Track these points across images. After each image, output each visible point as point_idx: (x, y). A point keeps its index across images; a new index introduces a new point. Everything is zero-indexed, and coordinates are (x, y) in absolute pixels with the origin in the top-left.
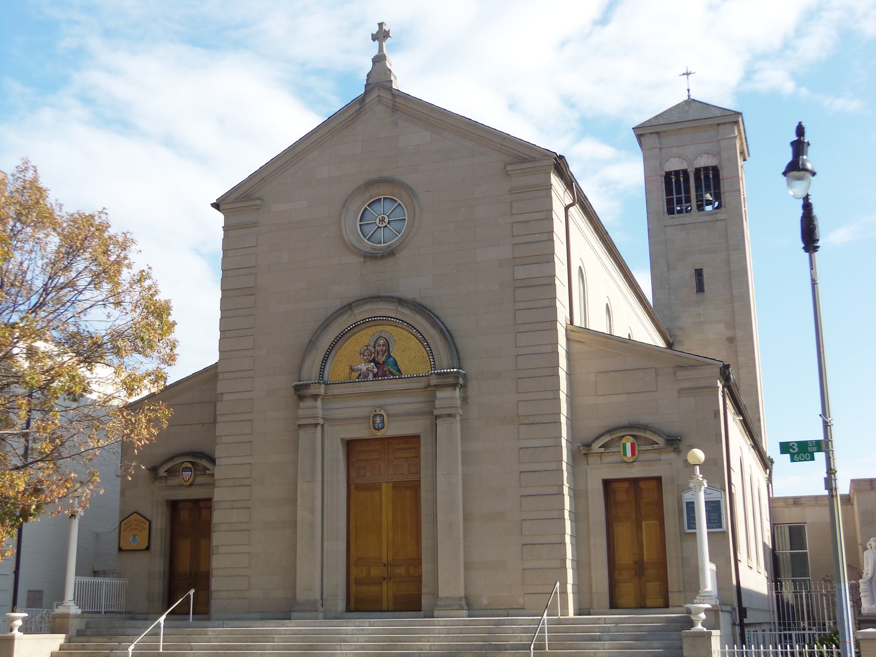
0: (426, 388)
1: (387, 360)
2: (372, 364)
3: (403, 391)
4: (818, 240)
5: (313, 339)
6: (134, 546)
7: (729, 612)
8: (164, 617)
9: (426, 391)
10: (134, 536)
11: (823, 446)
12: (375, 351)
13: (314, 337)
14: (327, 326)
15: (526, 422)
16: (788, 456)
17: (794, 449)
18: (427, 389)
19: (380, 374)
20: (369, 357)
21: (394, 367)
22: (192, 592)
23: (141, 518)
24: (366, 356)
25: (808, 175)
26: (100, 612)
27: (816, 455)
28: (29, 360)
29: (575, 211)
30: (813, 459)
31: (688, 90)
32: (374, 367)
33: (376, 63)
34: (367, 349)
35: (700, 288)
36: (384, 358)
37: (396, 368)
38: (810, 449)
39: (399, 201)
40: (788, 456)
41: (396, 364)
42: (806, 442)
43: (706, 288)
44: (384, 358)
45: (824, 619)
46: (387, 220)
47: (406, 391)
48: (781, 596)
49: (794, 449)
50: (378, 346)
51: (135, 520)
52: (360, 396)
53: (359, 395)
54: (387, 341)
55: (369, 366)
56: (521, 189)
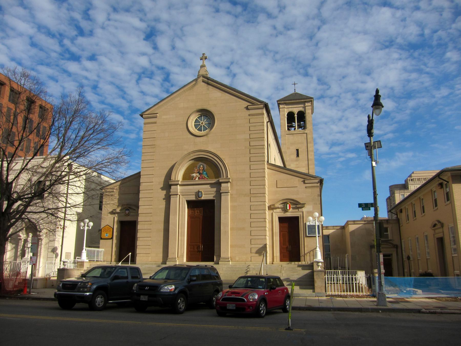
4: (373, 133)
6: (107, 237)
8: (121, 263)
10: (107, 233)
11: (374, 205)
16: (361, 208)
17: (363, 206)
19: (201, 177)
22: (130, 254)
25: (381, 107)
26: (94, 261)
27: (371, 208)
29: (269, 124)
30: (370, 209)
31: (295, 90)
33: (202, 68)
35: (298, 155)
38: (369, 206)
39: (209, 117)
40: (361, 208)
42: (361, 204)
43: (299, 156)
45: (338, 266)
46: (204, 123)
48: (344, 258)
49: (363, 206)
51: (107, 228)
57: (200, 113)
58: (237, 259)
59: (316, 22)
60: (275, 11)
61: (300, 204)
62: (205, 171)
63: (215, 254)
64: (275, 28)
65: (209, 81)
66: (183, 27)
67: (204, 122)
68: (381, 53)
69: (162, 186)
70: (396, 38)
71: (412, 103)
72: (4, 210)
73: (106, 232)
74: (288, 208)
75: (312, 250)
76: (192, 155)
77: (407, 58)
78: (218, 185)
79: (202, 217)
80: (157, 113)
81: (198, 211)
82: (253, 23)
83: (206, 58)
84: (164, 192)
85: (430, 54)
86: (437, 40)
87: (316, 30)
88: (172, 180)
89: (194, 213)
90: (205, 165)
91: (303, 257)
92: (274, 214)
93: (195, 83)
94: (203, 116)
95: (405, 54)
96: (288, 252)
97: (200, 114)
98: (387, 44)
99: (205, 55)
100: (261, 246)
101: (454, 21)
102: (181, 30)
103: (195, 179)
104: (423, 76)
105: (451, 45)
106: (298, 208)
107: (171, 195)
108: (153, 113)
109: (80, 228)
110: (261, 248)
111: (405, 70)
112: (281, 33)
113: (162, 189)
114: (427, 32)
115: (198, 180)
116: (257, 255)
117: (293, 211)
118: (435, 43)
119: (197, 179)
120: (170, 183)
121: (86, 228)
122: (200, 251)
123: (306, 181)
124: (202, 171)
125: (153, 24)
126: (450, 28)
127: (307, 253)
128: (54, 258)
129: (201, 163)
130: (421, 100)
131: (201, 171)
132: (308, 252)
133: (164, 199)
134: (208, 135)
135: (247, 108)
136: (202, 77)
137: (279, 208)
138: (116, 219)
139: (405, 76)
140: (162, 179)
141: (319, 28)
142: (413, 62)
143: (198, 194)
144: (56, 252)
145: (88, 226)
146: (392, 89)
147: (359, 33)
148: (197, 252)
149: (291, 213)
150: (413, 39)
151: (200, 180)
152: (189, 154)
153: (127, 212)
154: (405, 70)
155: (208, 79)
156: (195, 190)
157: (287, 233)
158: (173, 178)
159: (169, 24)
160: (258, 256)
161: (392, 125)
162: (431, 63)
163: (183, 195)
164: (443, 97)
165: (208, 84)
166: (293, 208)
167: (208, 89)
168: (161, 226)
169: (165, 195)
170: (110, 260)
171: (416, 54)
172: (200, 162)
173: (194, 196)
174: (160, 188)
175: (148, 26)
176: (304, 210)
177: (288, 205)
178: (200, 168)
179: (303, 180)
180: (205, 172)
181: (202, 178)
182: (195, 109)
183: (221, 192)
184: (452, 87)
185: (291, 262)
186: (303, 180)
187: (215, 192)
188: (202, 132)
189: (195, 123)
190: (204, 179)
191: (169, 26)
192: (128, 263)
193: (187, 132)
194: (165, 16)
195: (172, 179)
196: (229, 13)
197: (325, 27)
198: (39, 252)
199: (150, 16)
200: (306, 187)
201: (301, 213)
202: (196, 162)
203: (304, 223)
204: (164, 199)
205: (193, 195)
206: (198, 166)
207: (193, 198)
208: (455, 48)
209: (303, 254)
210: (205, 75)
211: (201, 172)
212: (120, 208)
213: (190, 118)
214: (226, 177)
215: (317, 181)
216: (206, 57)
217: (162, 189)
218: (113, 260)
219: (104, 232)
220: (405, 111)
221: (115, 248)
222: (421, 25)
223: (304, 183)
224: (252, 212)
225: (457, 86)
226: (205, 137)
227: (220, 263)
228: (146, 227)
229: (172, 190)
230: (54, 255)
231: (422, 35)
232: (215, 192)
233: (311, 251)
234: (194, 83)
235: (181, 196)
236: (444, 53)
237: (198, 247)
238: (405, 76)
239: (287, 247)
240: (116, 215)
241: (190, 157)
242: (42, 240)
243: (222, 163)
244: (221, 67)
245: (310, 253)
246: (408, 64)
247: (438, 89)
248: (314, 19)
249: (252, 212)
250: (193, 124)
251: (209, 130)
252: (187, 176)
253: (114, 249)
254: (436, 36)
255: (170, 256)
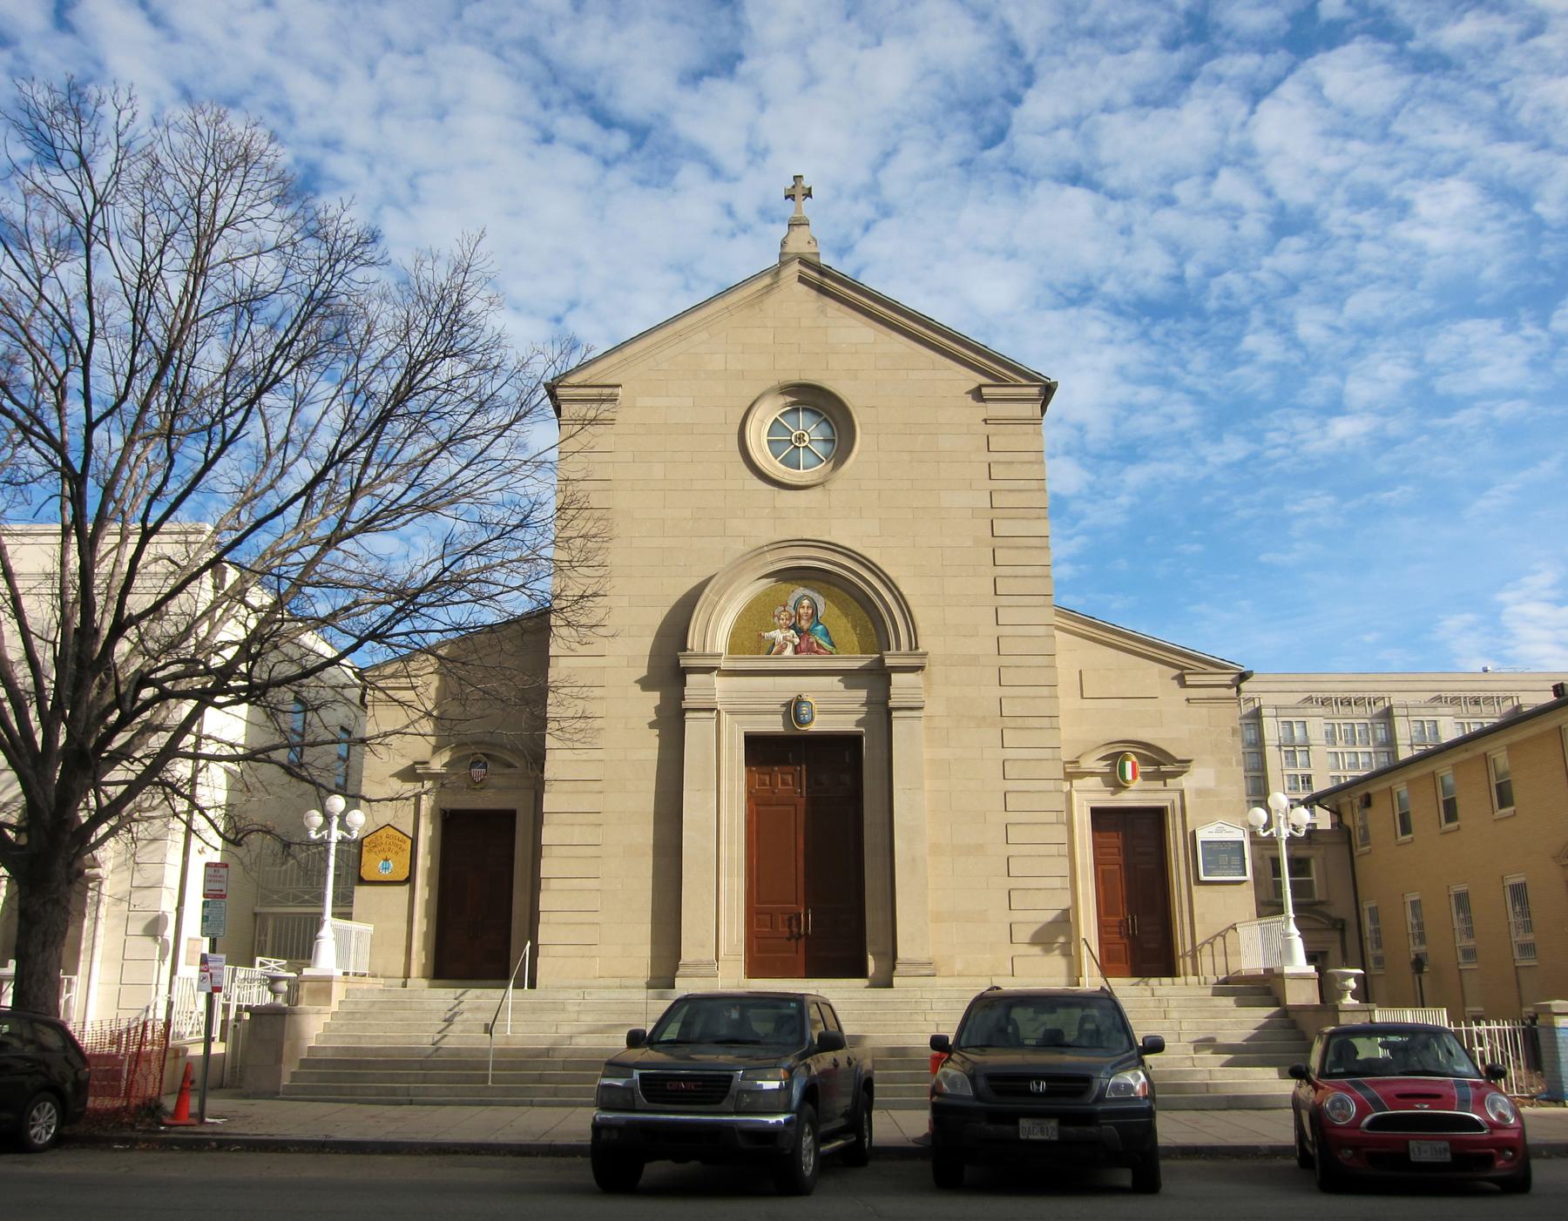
2: (792, 631)
6: (385, 875)
7: (551, 69)
10: (386, 860)
15: (1013, 725)
21: (824, 638)
23: (398, 834)
28: (355, 835)
33: (795, 228)
34: (785, 610)
39: (825, 416)
41: (827, 634)
46: (806, 438)
57: (790, 399)
58: (958, 966)
59: (864, 210)
60: (734, 161)
61: (1171, 759)
62: (818, 623)
63: (869, 948)
64: (730, 211)
65: (827, 280)
66: (416, 174)
67: (811, 430)
68: (1055, 320)
69: (643, 672)
70: (1102, 281)
71: (1135, 476)
72: (40, 746)
73: (383, 855)
74: (1129, 776)
75: (1219, 935)
76: (769, 557)
77: (1130, 341)
78: (877, 678)
79: (803, 800)
80: (618, 386)
81: (789, 778)
82: (658, 186)
83: (808, 194)
84: (654, 698)
85: (1197, 334)
86: (1218, 298)
87: (857, 231)
88: (688, 652)
89: (771, 785)
90: (821, 602)
91: (1189, 960)
92: (1075, 794)
93: (772, 284)
94: (804, 410)
95: (1126, 329)
96: (1125, 941)
97: (792, 404)
98: (1074, 293)
99: (806, 183)
100: (1049, 916)
101: (1269, 250)
102: (412, 185)
103: (779, 652)
104: (1177, 396)
105: (1257, 317)
106: (1164, 776)
107: (686, 709)
108: (599, 383)
109: (309, 837)
110: (1050, 923)
111: (1121, 372)
112: (745, 229)
113: (646, 684)
114: (1192, 271)
115: (792, 655)
116: (1037, 950)
117: (1147, 788)
118: (1212, 304)
119: (789, 651)
120: (683, 663)
121: (336, 834)
122: (799, 937)
123: (1187, 678)
124: (808, 620)
125: (313, 154)
126: (1259, 268)
127: (1203, 944)
128: (156, 963)
129: (800, 591)
130: (1166, 468)
131: (803, 622)
132: (1206, 942)
133: (652, 725)
134: (828, 486)
135: (977, 394)
136: (800, 262)
137: (1092, 774)
138: (426, 803)
139: (1123, 392)
140: (645, 644)
141: (867, 228)
142: (1149, 354)
143: (793, 710)
144: (162, 936)
145: (343, 825)
146: (1081, 428)
147: (992, 253)
148: (789, 939)
149: (1137, 794)
150: (1152, 286)
151: (803, 655)
152: (760, 551)
153: (477, 772)
154: (1121, 372)
155: (823, 271)
156: (785, 694)
157: (1117, 867)
158: (693, 641)
159: (370, 160)
160: (1040, 953)
161: (1070, 538)
162: (1199, 360)
163: (731, 713)
164: (1229, 466)
165: (822, 290)
166: (1147, 777)
167: (823, 312)
168: (644, 835)
169: (658, 710)
170: (401, 973)
171: (1158, 332)
172: (800, 586)
173: (779, 718)
174: (636, 682)
175: (297, 161)
176: (1184, 782)
177: (1128, 765)
178: (801, 611)
179: (1177, 672)
180: (820, 627)
181: (810, 650)
182: (774, 383)
183: (891, 704)
184: (1256, 437)
185: (1146, 979)
186: (1177, 672)
187: (863, 705)
188: (802, 471)
189: (768, 435)
190: (817, 652)
191: (370, 167)
192: (503, 982)
193: (744, 466)
194: (359, 133)
195: (689, 646)
196: (584, 149)
197: (884, 225)
198: (84, 935)
199: (309, 127)
200: (1188, 700)
201: (1176, 796)
202: (783, 586)
203: (1190, 830)
204: (652, 725)
205: (774, 713)
206: (791, 603)
207: (773, 725)
208: (1270, 323)
209: (1188, 947)
210: (808, 256)
211: (804, 624)
212: (446, 757)
213: (753, 412)
214: (911, 649)
215: (1227, 679)
216: (810, 189)
217: (646, 684)
218: (416, 969)
219: (373, 855)
220: (1113, 498)
221: (425, 921)
222: (1177, 250)
223: (1183, 684)
224: (1009, 785)
225: (1271, 436)
226: (818, 490)
227: (896, 981)
228: (577, 835)
229: (898, 691)
230: (158, 948)
231: (1179, 279)
232: (863, 705)
233: (1215, 937)
234: (767, 281)
235: (723, 714)
236: (1237, 338)
237: (790, 920)
238: (1123, 392)
239: (1121, 922)
240: (428, 784)
241: (766, 564)
242: (101, 883)
243: (891, 596)
244: (533, 313)
245: (1212, 944)
246: (1134, 355)
247: (1216, 438)
248: (856, 197)
249: (1009, 785)
250: (765, 438)
251: (831, 464)
252: (749, 637)
253: (420, 925)
254: (1216, 285)
255: (688, 954)
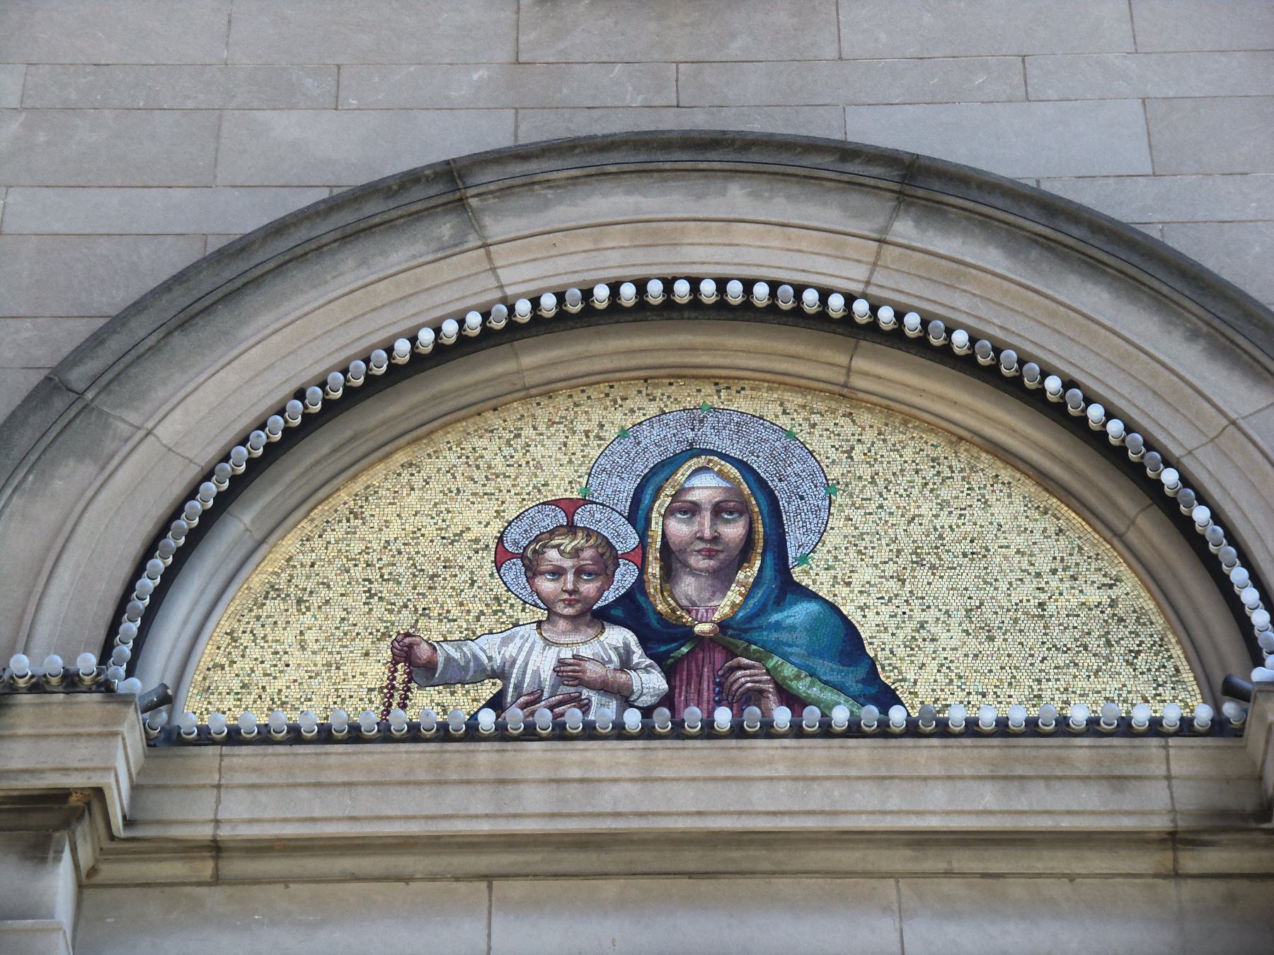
0: (1174, 840)
1: (762, 611)
2: (618, 636)
3: (933, 861)
5: (77, 377)
9: (1177, 875)
12: (643, 544)
13: (92, 366)
14: (232, 295)
18: (1191, 861)
20: (589, 588)
24: (558, 573)
32: (638, 655)
34: (571, 529)
36: (734, 595)
37: (852, 676)
44: (734, 595)
47: (966, 860)
50: (670, 512)
52: (488, 878)
53: (484, 862)
54: (762, 483)
55: (585, 651)
56: (476, 384)
